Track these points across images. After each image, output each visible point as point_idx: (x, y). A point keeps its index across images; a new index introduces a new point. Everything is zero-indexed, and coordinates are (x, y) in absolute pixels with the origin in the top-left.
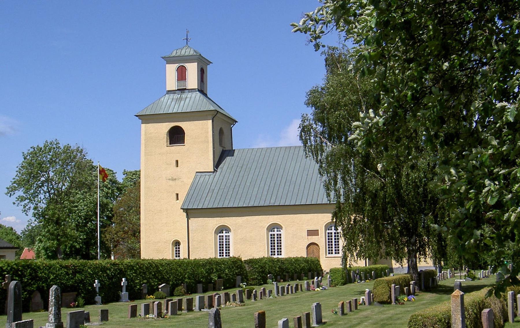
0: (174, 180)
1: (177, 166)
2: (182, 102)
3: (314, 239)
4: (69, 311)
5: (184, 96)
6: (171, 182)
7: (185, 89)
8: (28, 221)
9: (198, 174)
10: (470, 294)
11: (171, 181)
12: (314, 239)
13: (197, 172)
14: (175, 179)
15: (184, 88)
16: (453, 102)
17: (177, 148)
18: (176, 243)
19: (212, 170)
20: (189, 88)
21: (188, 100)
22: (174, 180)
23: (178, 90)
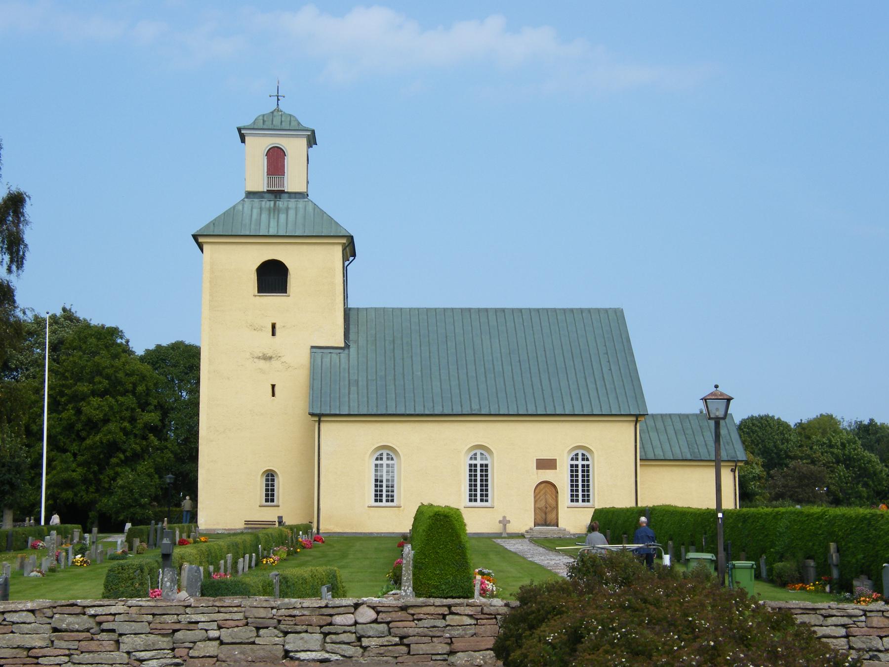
0: (267, 358)
1: (273, 334)
2: (283, 217)
3: (547, 475)
4: (773, 599)
5: (281, 204)
6: (262, 364)
7: (283, 192)
8: (759, 594)
9: (315, 350)
10: (537, 548)
11: (262, 362)
12: (547, 475)
13: (313, 347)
14: (271, 358)
15: (280, 189)
16: (805, 521)
17: (273, 300)
18: (268, 476)
19: (342, 345)
20: (290, 190)
21: (292, 213)
22: (267, 358)
23: (269, 192)
